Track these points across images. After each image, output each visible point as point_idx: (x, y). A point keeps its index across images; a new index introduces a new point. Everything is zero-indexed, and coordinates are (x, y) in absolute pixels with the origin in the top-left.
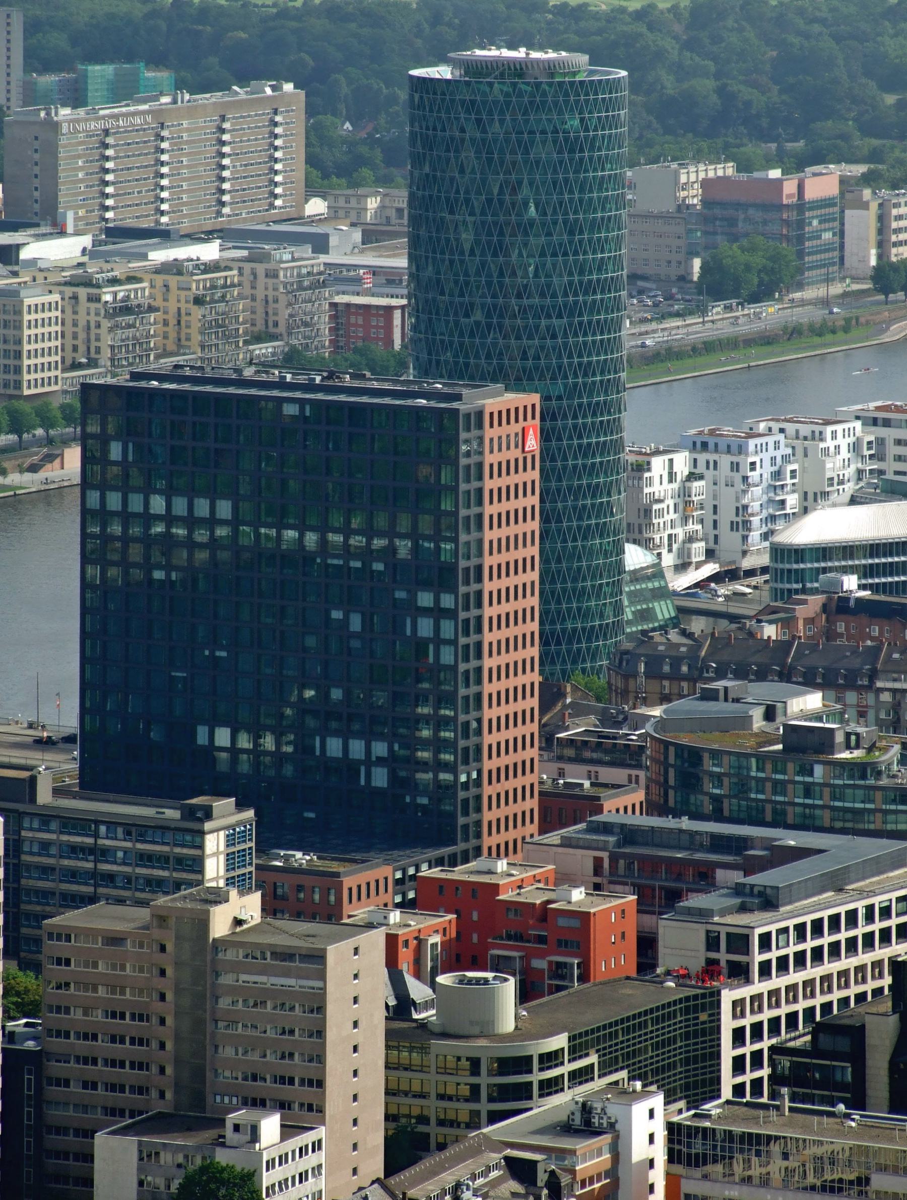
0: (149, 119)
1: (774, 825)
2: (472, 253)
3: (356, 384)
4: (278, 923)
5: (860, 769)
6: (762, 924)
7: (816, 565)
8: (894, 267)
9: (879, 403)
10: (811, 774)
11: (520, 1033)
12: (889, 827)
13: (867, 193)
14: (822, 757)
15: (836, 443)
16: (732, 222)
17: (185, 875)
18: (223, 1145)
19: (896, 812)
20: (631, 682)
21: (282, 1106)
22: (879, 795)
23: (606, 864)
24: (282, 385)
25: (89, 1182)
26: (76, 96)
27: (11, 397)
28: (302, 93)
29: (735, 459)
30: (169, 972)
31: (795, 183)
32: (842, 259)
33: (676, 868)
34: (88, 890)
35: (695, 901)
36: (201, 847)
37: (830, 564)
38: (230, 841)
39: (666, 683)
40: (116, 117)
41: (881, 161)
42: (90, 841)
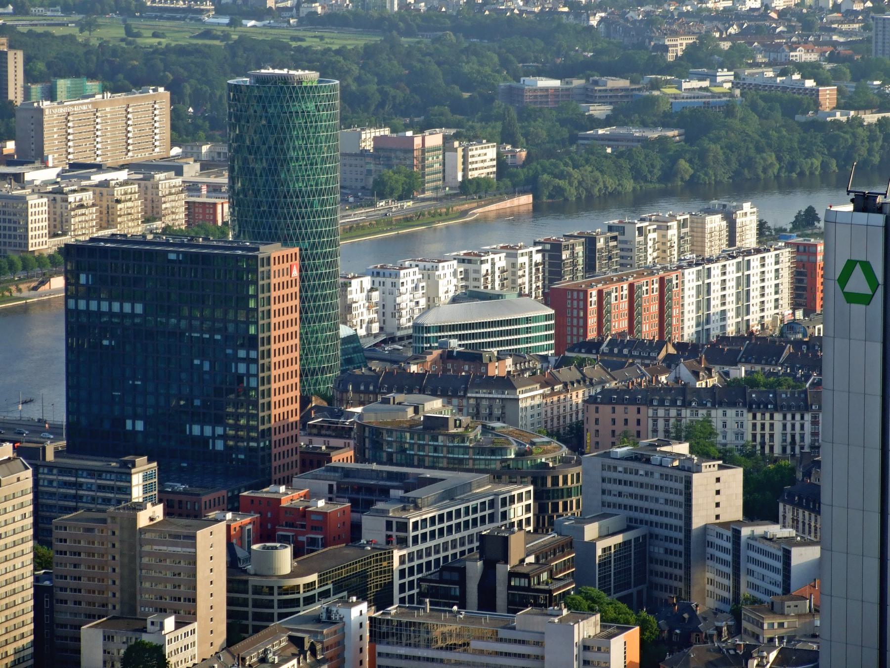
0: (90, 106)
1: (418, 466)
2: (261, 176)
3: (205, 243)
4: (172, 520)
5: (462, 438)
6: (414, 517)
7: (436, 334)
8: (471, 181)
9: (465, 252)
10: (437, 441)
11: (293, 574)
12: (476, 467)
13: (456, 144)
14: (443, 432)
15: (444, 272)
16: (389, 158)
17: (122, 496)
18: (146, 632)
19: (480, 459)
20: (344, 395)
21: (176, 612)
22: (471, 451)
23: (335, 488)
24: (167, 244)
25: (78, 651)
26: (51, 95)
27: (22, 251)
28: (168, 93)
29: (394, 280)
30: (117, 545)
31: (420, 138)
32: (444, 177)
33: (370, 489)
34: (73, 504)
35: (380, 505)
36: (130, 482)
37: (443, 334)
38: (145, 478)
39: (362, 395)
40: (73, 106)
41: (462, 127)
42: (73, 479)
